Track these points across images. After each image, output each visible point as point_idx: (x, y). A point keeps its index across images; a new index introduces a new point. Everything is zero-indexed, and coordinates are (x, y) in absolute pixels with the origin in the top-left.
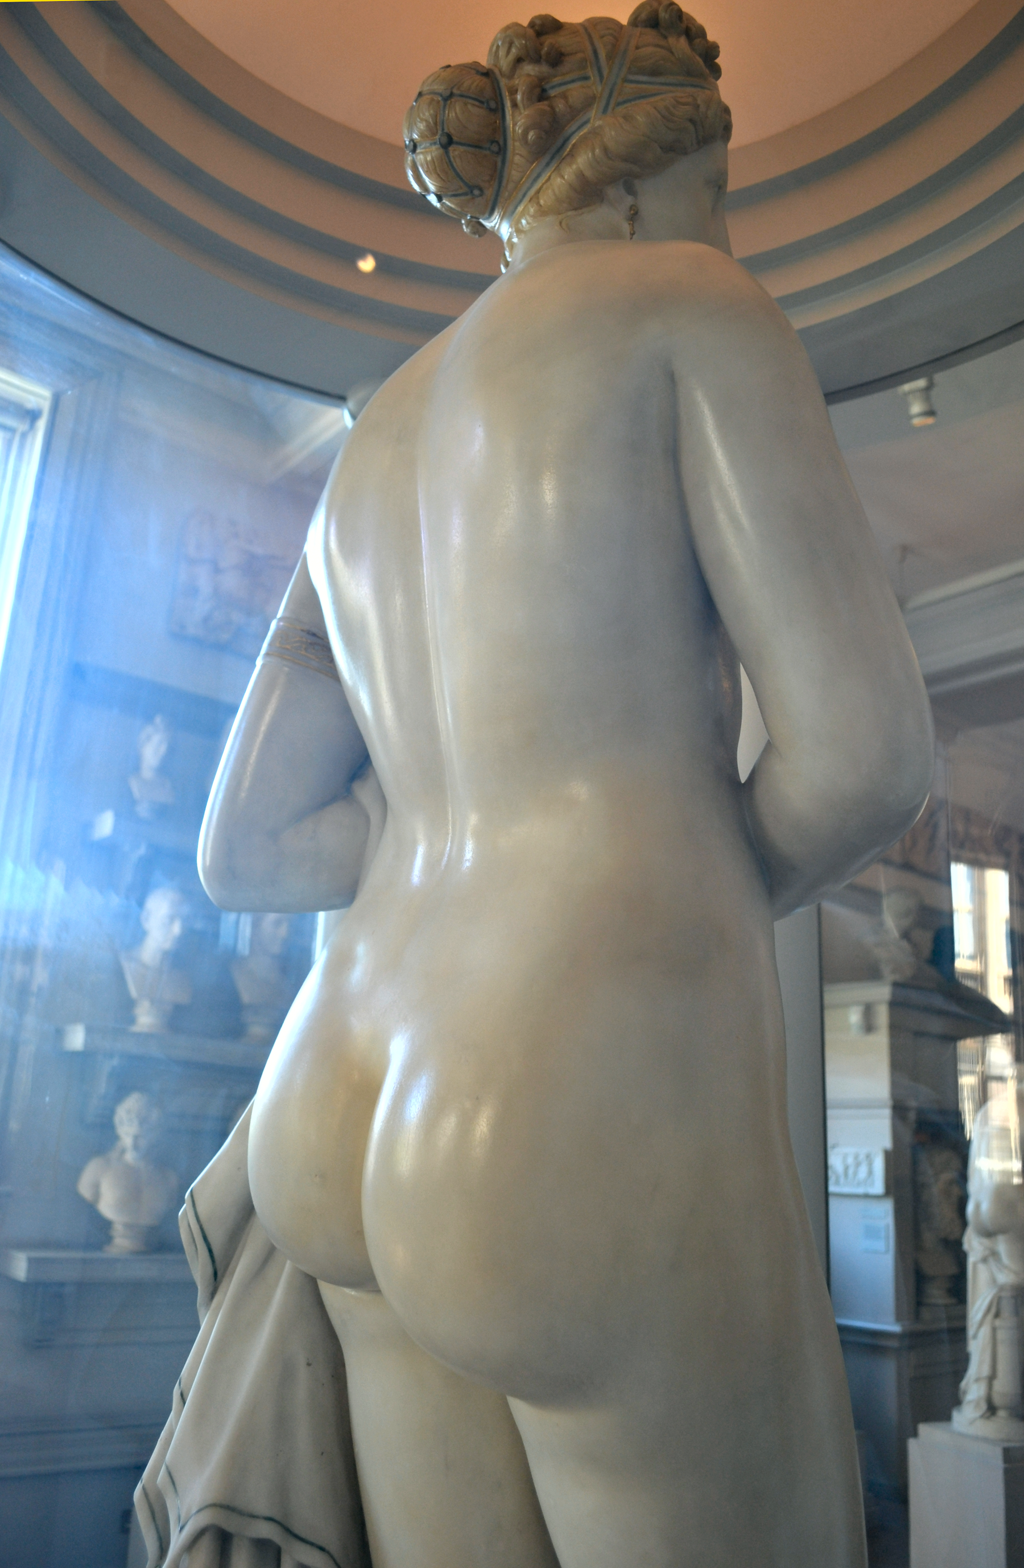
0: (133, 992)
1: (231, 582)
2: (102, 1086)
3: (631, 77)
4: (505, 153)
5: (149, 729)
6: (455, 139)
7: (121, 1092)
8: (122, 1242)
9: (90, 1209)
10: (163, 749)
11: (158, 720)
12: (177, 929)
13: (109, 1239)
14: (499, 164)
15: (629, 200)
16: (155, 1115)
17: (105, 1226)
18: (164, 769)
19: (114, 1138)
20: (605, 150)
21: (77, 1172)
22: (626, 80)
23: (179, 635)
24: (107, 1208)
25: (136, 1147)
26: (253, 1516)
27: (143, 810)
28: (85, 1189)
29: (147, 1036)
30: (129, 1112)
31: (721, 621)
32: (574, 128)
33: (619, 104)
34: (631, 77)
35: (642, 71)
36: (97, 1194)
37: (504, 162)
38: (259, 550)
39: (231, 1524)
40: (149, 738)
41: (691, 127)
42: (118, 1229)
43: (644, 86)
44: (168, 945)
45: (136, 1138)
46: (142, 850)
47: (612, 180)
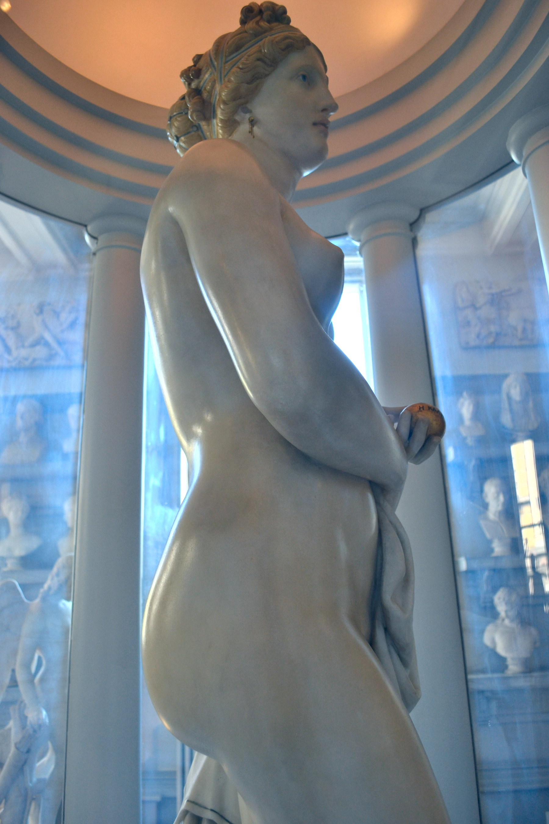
0: (488, 536)
1: (487, 312)
2: (484, 587)
3: (228, 59)
4: (201, 128)
5: (461, 400)
6: (179, 136)
7: (495, 590)
8: (513, 668)
9: (493, 652)
10: (471, 408)
11: (465, 394)
12: (501, 498)
13: (506, 667)
14: (201, 134)
15: (248, 116)
16: (514, 597)
17: (503, 660)
20: (225, 103)
22: (226, 62)
23: (467, 348)
24: (501, 650)
26: (206, 808)
28: (487, 640)
30: (499, 599)
32: (214, 99)
33: (225, 76)
34: (228, 59)
35: (231, 53)
37: (202, 132)
38: (494, 291)
39: (197, 811)
40: (463, 404)
41: (259, 63)
42: (509, 662)
43: (235, 59)
44: (500, 508)
45: (506, 612)
46: (473, 463)
47: (235, 112)
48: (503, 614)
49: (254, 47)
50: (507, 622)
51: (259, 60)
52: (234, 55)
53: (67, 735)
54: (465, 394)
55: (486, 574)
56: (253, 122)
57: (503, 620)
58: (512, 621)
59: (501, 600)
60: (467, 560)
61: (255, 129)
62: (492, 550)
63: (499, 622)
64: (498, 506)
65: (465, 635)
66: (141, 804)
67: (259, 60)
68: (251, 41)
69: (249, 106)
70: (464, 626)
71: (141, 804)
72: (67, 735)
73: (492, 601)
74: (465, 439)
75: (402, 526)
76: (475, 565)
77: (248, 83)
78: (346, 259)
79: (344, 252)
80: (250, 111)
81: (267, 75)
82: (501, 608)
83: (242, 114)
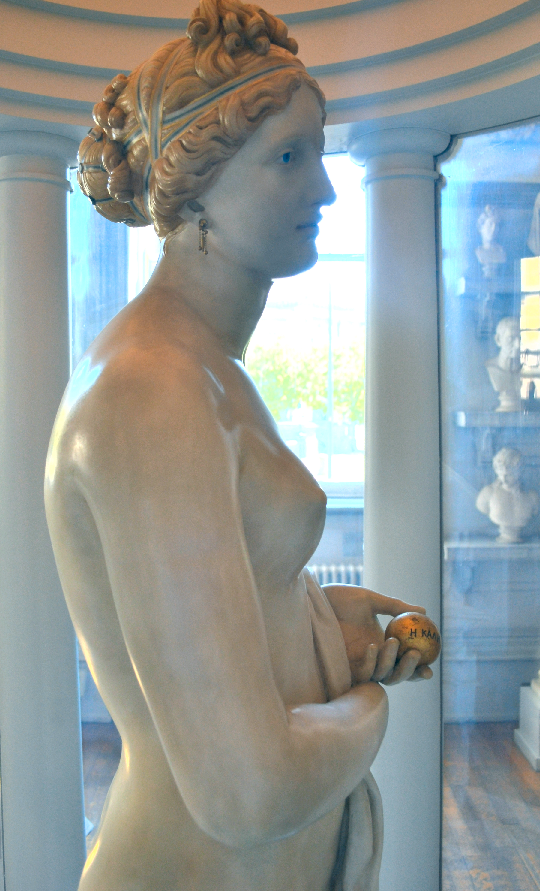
6: (96, 199)
8: (505, 537)
9: (485, 517)
10: (493, 228)
11: (487, 208)
15: (198, 216)
16: (516, 461)
17: (496, 527)
18: (497, 239)
19: (496, 476)
21: (473, 502)
22: (164, 122)
24: (495, 516)
25: (506, 481)
27: (487, 271)
29: (505, 415)
30: (499, 461)
31: (110, 785)
36: (488, 509)
40: (483, 223)
41: (214, 144)
43: (177, 121)
45: (506, 476)
48: (501, 477)
49: (207, 106)
50: (505, 486)
51: (215, 138)
52: (178, 113)
53: (2, 809)
54: (487, 208)
55: (488, 431)
56: (204, 226)
57: (501, 484)
58: (511, 486)
59: (502, 463)
60: (468, 417)
61: (210, 234)
62: (498, 403)
63: (495, 485)
64: (511, 352)
65: (444, 686)
66: (78, 664)
67: (215, 138)
68: (202, 94)
69: (200, 201)
70: (445, 677)
71: (78, 664)
72: (2, 809)
73: (491, 462)
74: (482, 266)
75: (375, 784)
76: (478, 422)
77: (198, 174)
78: (329, 500)
79: (327, 495)
80: (201, 209)
81: (227, 159)
82: (501, 472)
83: (190, 212)
